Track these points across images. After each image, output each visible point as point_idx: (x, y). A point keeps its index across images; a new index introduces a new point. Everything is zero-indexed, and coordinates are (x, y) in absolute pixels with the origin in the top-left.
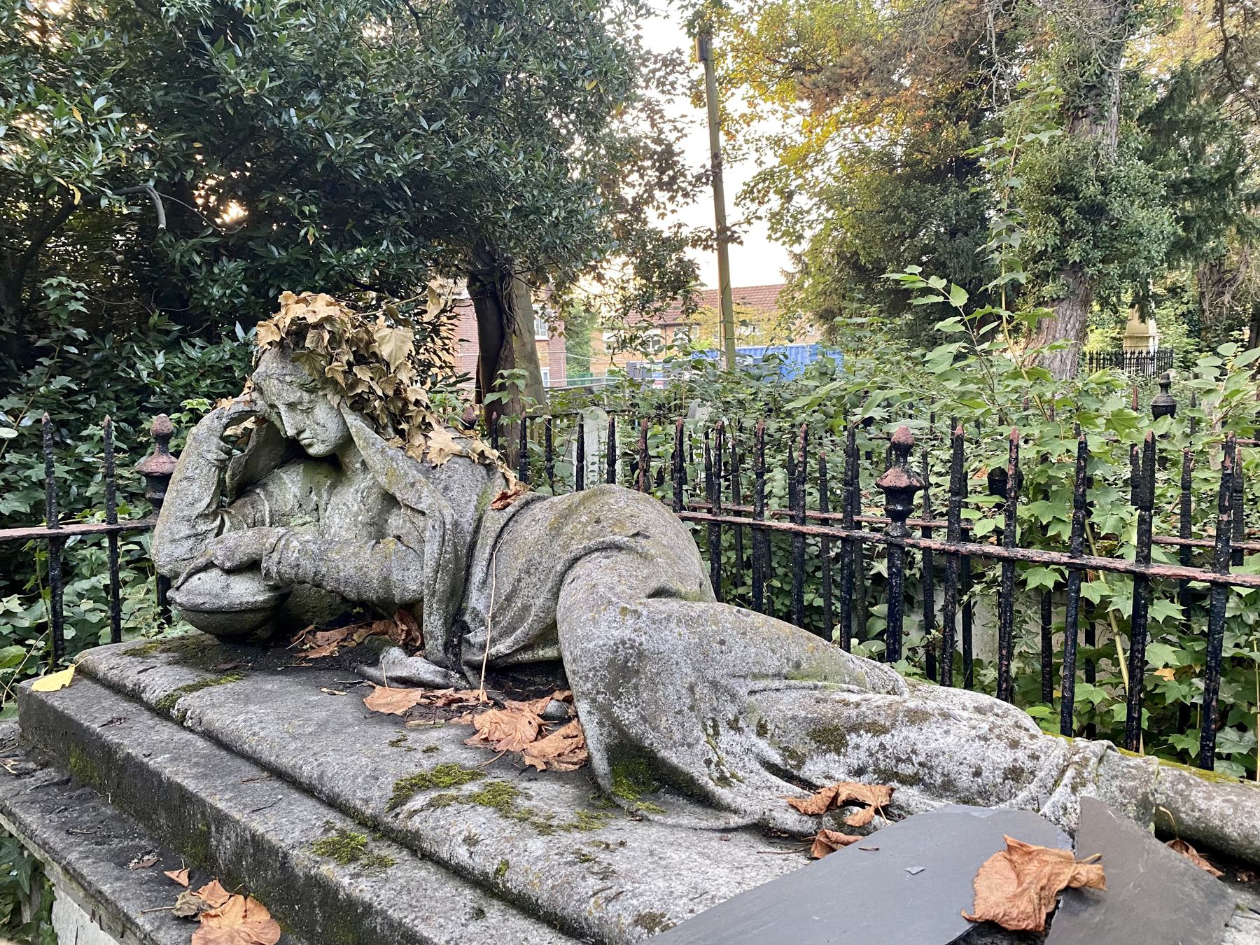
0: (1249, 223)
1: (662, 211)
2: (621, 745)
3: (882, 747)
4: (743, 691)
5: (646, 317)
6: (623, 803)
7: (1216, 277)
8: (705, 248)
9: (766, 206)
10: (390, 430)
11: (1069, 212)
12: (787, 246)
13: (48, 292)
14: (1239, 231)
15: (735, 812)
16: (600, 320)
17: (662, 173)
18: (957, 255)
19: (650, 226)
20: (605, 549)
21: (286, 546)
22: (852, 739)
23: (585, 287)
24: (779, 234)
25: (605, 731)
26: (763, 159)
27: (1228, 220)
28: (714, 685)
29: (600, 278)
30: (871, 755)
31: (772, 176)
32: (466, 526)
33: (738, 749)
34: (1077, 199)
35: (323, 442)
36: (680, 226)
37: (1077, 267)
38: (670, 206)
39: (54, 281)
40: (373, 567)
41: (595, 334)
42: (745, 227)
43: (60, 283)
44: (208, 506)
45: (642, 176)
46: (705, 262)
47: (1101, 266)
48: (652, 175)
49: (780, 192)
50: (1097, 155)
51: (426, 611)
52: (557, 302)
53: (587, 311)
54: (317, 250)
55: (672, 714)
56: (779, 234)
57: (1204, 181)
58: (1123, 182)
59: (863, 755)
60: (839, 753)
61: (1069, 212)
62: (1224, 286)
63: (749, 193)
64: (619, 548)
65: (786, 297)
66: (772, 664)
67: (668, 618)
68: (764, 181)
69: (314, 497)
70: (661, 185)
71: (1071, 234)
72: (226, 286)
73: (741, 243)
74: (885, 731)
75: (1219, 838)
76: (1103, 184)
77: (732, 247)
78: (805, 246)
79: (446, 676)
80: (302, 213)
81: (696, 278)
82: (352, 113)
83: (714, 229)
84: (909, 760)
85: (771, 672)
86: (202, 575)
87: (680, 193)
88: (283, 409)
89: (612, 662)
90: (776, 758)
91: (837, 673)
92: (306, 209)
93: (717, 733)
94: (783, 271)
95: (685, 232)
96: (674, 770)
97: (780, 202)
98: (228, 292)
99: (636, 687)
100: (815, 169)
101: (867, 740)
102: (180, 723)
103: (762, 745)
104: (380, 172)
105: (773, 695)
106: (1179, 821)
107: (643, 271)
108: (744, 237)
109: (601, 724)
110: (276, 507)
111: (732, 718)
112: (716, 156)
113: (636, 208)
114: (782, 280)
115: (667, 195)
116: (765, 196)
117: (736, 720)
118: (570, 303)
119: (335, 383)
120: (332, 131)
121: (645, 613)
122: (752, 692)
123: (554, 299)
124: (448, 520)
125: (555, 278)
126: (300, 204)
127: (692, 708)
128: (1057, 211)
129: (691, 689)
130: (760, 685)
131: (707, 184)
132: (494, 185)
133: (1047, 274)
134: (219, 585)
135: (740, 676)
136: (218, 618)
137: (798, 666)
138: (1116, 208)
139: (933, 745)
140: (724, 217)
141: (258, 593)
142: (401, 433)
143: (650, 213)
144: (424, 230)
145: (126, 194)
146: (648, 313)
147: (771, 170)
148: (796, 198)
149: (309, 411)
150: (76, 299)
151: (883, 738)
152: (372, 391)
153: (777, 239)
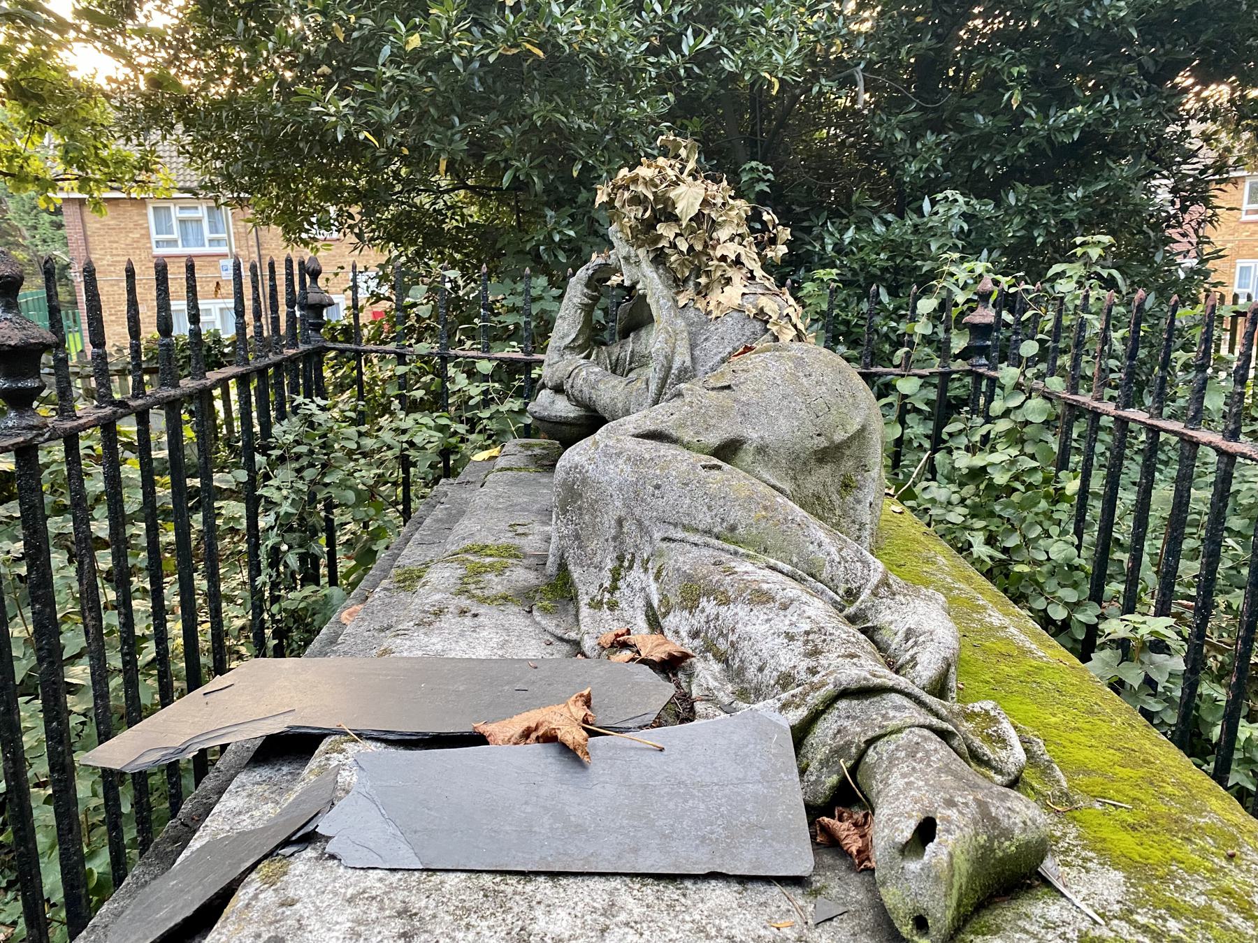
22: (703, 602)
28: (640, 523)
30: (707, 622)
33: (637, 586)
44: (573, 340)
55: (602, 540)
67: (619, 455)
85: (701, 527)
91: (781, 549)
93: (630, 567)
98: (925, 166)
103: (653, 588)
110: (637, 349)
117: (648, 561)
124: (676, 365)
129: (620, 522)
130: (679, 534)
137: (733, 528)
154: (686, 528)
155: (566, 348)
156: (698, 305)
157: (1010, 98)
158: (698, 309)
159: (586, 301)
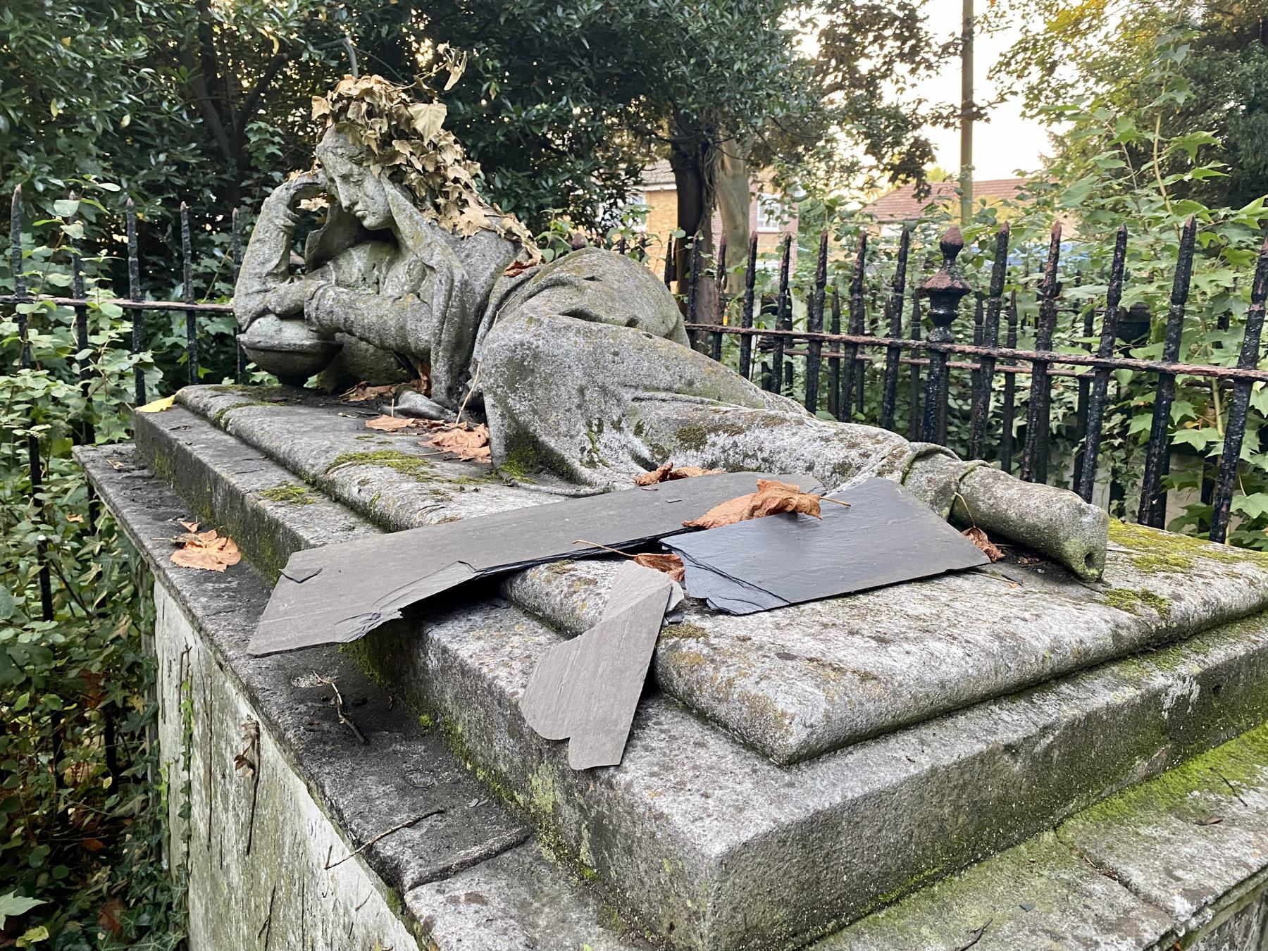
1: (900, 85)
2: (518, 435)
3: (735, 445)
4: (627, 395)
6: (505, 476)
8: (947, 126)
9: (1025, 80)
10: (428, 204)
12: (1045, 124)
15: (590, 484)
18: (1252, 135)
20: (553, 286)
21: (323, 295)
22: (711, 438)
24: (1035, 111)
25: (506, 422)
28: (603, 390)
30: (724, 452)
32: (478, 289)
33: (616, 445)
35: (374, 214)
36: (920, 102)
38: (911, 79)
39: (255, 126)
40: (391, 316)
43: (260, 128)
44: (277, 266)
45: (882, 47)
46: (945, 142)
49: (1041, 62)
51: (433, 357)
56: (1035, 111)
59: (717, 451)
60: (697, 450)
66: (665, 378)
68: (1025, 50)
69: (376, 272)
70: (902, 56)
73: (988, 120)
74: (740, 431)
75: (1004, 521)
77: (977, 125)
79: (442, 412)
80: (486, 69)
81: (933, 159)
84: (755, 456)
85: (662, 385)
86: (261, 320)
87: (923, 66)
88: (338, 180)
89: (511, 360)
90: (646, 453)
92: (490, 64)
93: (600, 431)
95: (923, 110)
96: (551, 452)
97: (1040, 74)
99: (531, 384)
100: (1090, 36)
101: (723, 439)
102: (224, 430)
105: (658, 404)
106: (977, 509)
109: (502, 415)
111: (615, 418)
112: (968, 21)
113: (871, 82)
115: (908, 67)
116: (1025, 68)
117: (620, 421)
121: (546, 321)
122: (636, 399)
124: (457, 278)
127: (579, 407)
129: (581, 391)
131: (955, 54)
134: (274, 328)
135: (631, 386)
136: (272, 356)
137: (690, 383)
139: (778, 443)
140: (971, 92)
141: (307, 339)
142: (437, 207)
145: (326, 48)
149: (359, 183)
150: (274, 143)
151: (736, 438)
152: (410, 164)
153: (1032, 117)
154: (646, 389)
155: (269, 274)
156: (443, 225)
157: (488, 89)
158: (444, 229)
159: (290, 223)
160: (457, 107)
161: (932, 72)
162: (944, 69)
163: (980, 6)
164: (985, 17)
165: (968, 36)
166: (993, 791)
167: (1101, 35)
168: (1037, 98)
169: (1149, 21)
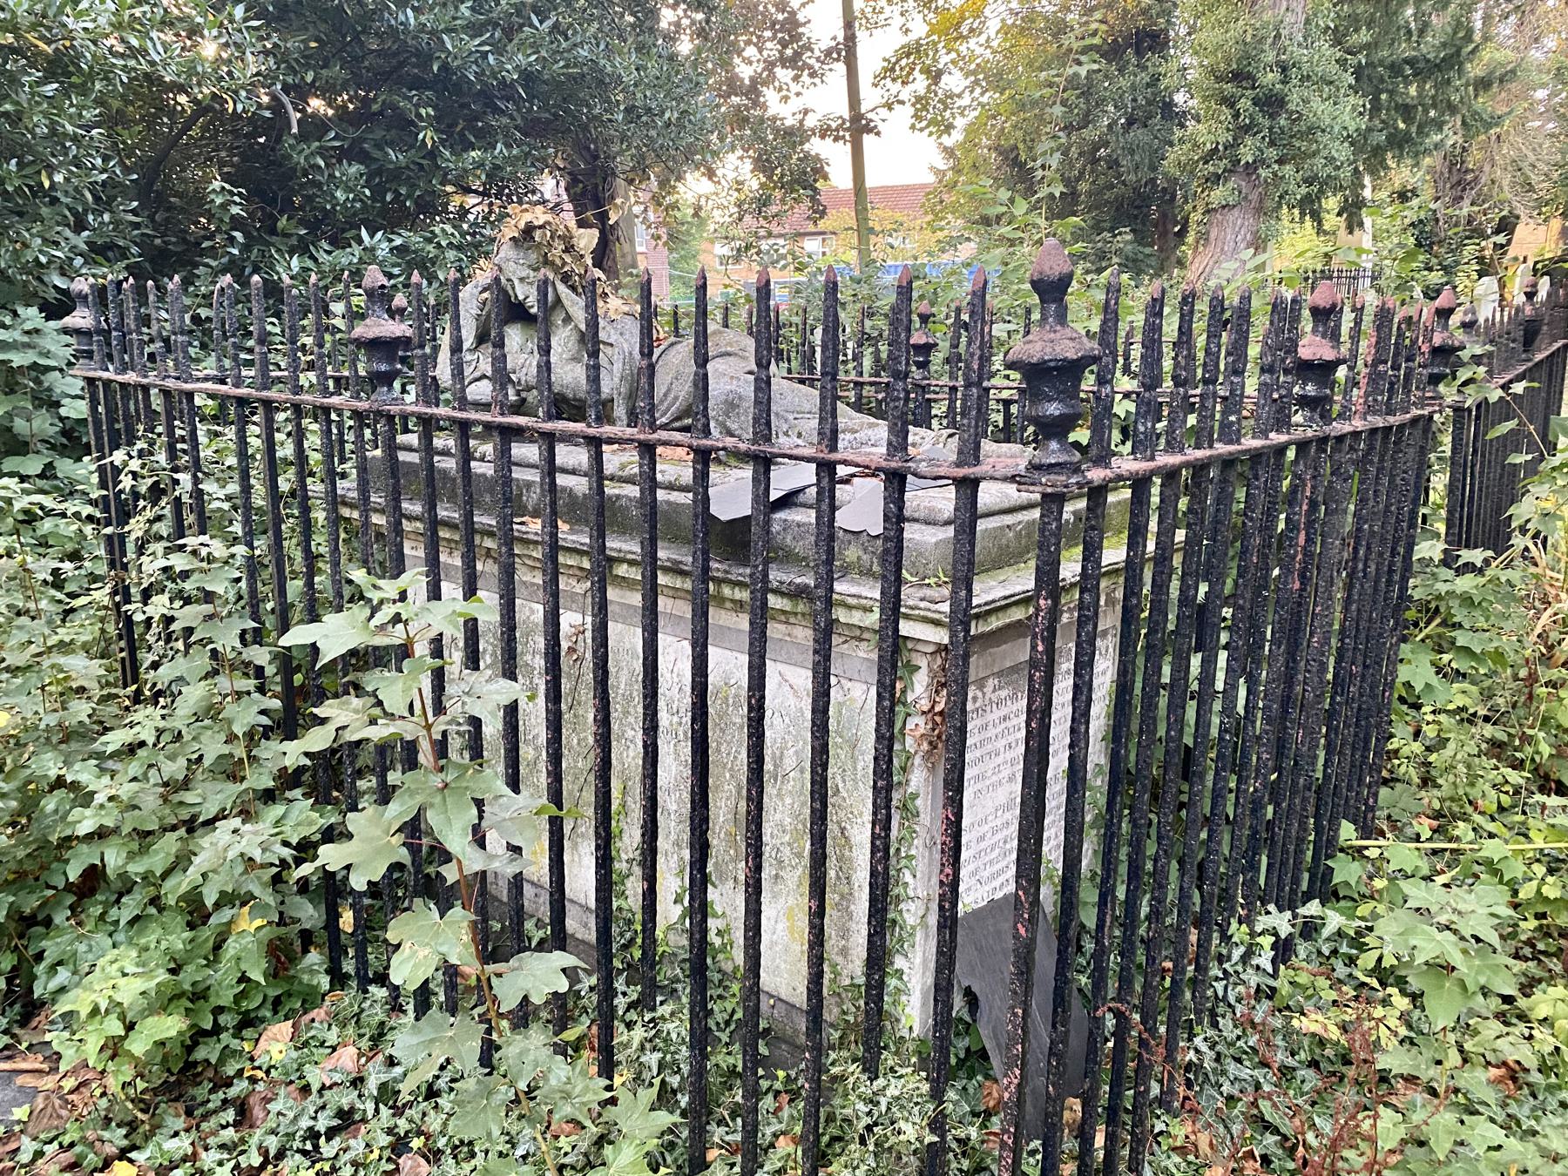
0: (1476, 113)
1: (784, 93)
4: (791, 417)
5: (763, 222)
7: (1455, 179)
8: (836, 139)
9: (911, 87)
11: (1244, 104)
13: (213, 196)
14: (1464, 123)
16: (712, 227)
17: (785, 46)
18: (1132, 152)
19: (770, 112)
23: (693, 186)
24: (924, 123)
26: (909, 25)
27: (1452, 109)
29: (711, 174)
31: (918, 51)
34: (1254, 88)
36: (806, 112)
37: (1251, 169)
38: (794, 88)
41: (704, 245)
42: (883, 112)
45: (760, 51)
46: (835, 157)
47: (1276, 167)
48: (772, 49)
49: (926, 71)
50: (1278, 36)
52: (660, 205)
53: (696, 215)
54: (433, 154)
56: (924, 123)
57: (1428, 61)
58: (1305, 67)
61: (1244, 104)
62: (1464, 189)
63: (889, 71)
64: (729, 354)
65: (934, 201)
68: (908, 55)
70: (784, 62)
71: (1246, 129)
72: (348, 190)
73: (878, 134)
76: (1284, 70)
77: (868, 140)
78: (956, 137)
80: (419, 116)
81: (826, 177)
82: (467, 13)
83: (847, 116)
88: (516, 282)
92: (423, 111)
94: (932, 168)
97: (926, 83)
104: (494, 75)
107: (763, 165)
108: (881, 127)
112: (849, 25)
113: (753, 91)
114: (931, 179)
115: (791, 73)
116: (909, 74)
118: (674, 206)
119: (553, 263)
120: (448, 31)
123: (657, 200)
125: (657, 176)
126: (417, 106)
128: (1230, 102)
131: (838, 60)
132: (602, 83)
133: (1218, 177)
138: (1294, 100)
143: (770, 96)
144: (534, 129)
146: (765, 218)
147: (917, 42)
148: (945, 78)
153: (921, 130)
160: (387, 154)
161: (817, 80)
162: (829, 77)
163: (858, 3)
164: (863, 12)
165: (850, 39)
166: (1004, 541)
167: (982, 39)
168: (925, 108)
169: (1025, 25)
